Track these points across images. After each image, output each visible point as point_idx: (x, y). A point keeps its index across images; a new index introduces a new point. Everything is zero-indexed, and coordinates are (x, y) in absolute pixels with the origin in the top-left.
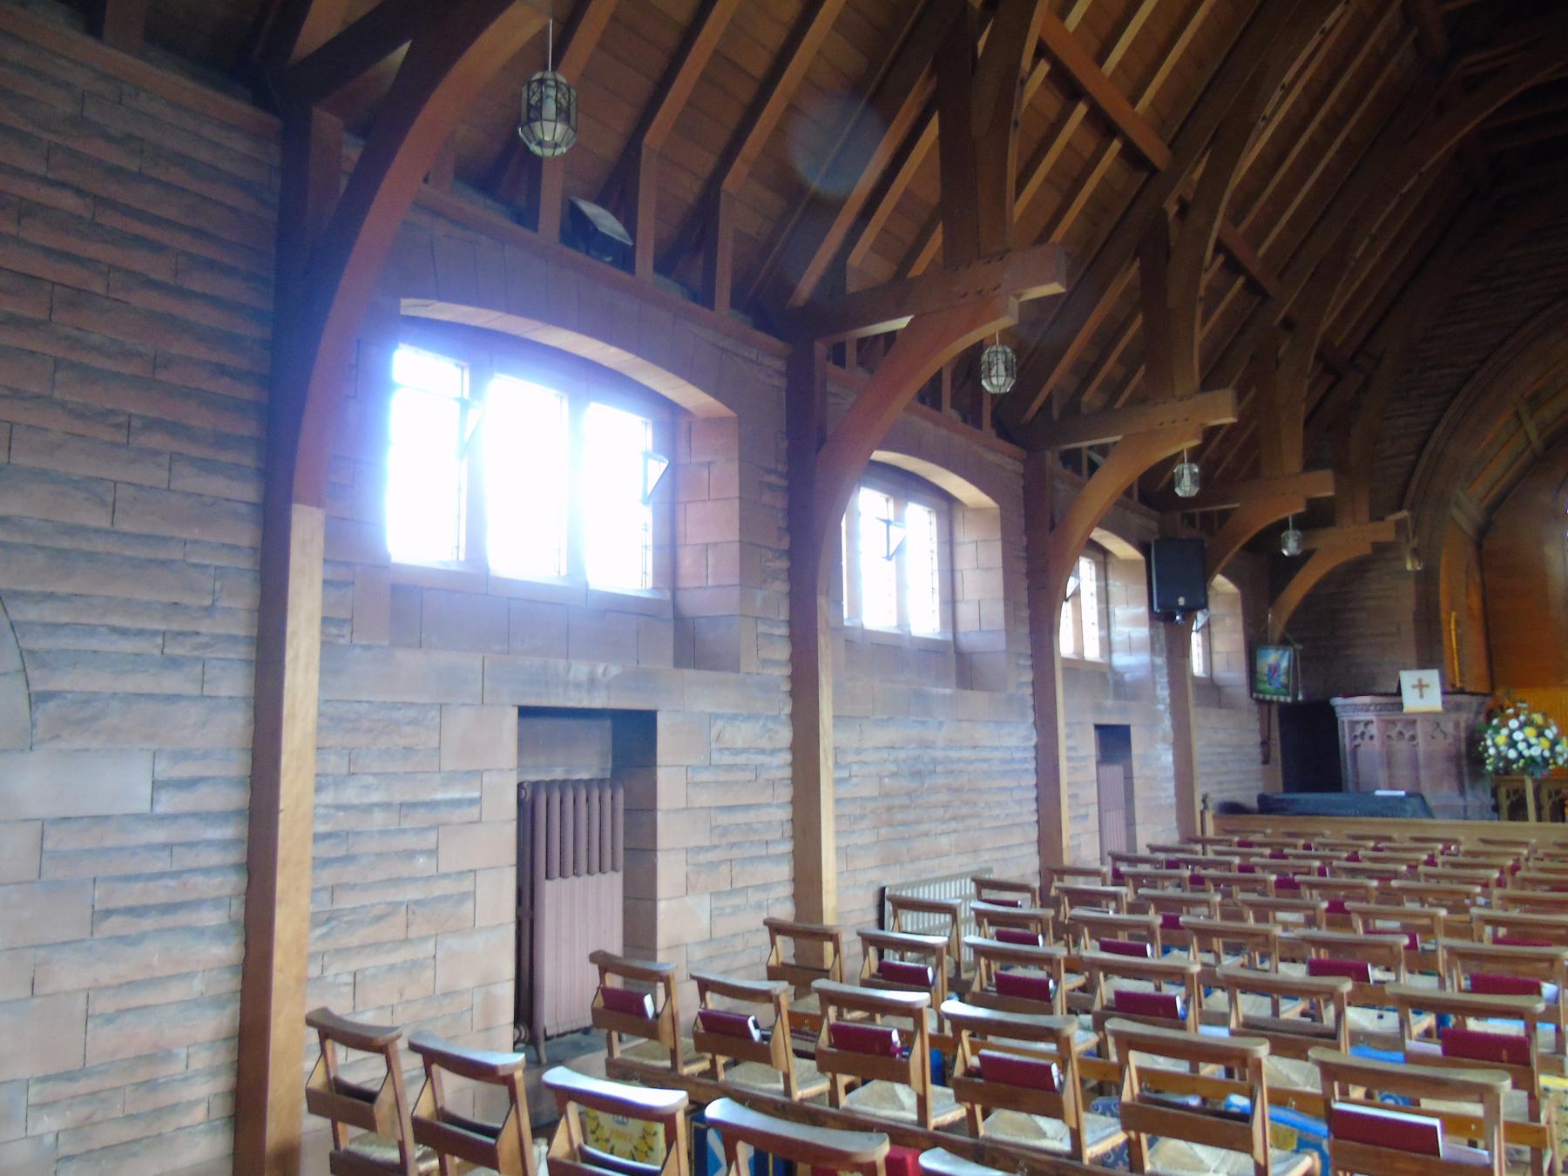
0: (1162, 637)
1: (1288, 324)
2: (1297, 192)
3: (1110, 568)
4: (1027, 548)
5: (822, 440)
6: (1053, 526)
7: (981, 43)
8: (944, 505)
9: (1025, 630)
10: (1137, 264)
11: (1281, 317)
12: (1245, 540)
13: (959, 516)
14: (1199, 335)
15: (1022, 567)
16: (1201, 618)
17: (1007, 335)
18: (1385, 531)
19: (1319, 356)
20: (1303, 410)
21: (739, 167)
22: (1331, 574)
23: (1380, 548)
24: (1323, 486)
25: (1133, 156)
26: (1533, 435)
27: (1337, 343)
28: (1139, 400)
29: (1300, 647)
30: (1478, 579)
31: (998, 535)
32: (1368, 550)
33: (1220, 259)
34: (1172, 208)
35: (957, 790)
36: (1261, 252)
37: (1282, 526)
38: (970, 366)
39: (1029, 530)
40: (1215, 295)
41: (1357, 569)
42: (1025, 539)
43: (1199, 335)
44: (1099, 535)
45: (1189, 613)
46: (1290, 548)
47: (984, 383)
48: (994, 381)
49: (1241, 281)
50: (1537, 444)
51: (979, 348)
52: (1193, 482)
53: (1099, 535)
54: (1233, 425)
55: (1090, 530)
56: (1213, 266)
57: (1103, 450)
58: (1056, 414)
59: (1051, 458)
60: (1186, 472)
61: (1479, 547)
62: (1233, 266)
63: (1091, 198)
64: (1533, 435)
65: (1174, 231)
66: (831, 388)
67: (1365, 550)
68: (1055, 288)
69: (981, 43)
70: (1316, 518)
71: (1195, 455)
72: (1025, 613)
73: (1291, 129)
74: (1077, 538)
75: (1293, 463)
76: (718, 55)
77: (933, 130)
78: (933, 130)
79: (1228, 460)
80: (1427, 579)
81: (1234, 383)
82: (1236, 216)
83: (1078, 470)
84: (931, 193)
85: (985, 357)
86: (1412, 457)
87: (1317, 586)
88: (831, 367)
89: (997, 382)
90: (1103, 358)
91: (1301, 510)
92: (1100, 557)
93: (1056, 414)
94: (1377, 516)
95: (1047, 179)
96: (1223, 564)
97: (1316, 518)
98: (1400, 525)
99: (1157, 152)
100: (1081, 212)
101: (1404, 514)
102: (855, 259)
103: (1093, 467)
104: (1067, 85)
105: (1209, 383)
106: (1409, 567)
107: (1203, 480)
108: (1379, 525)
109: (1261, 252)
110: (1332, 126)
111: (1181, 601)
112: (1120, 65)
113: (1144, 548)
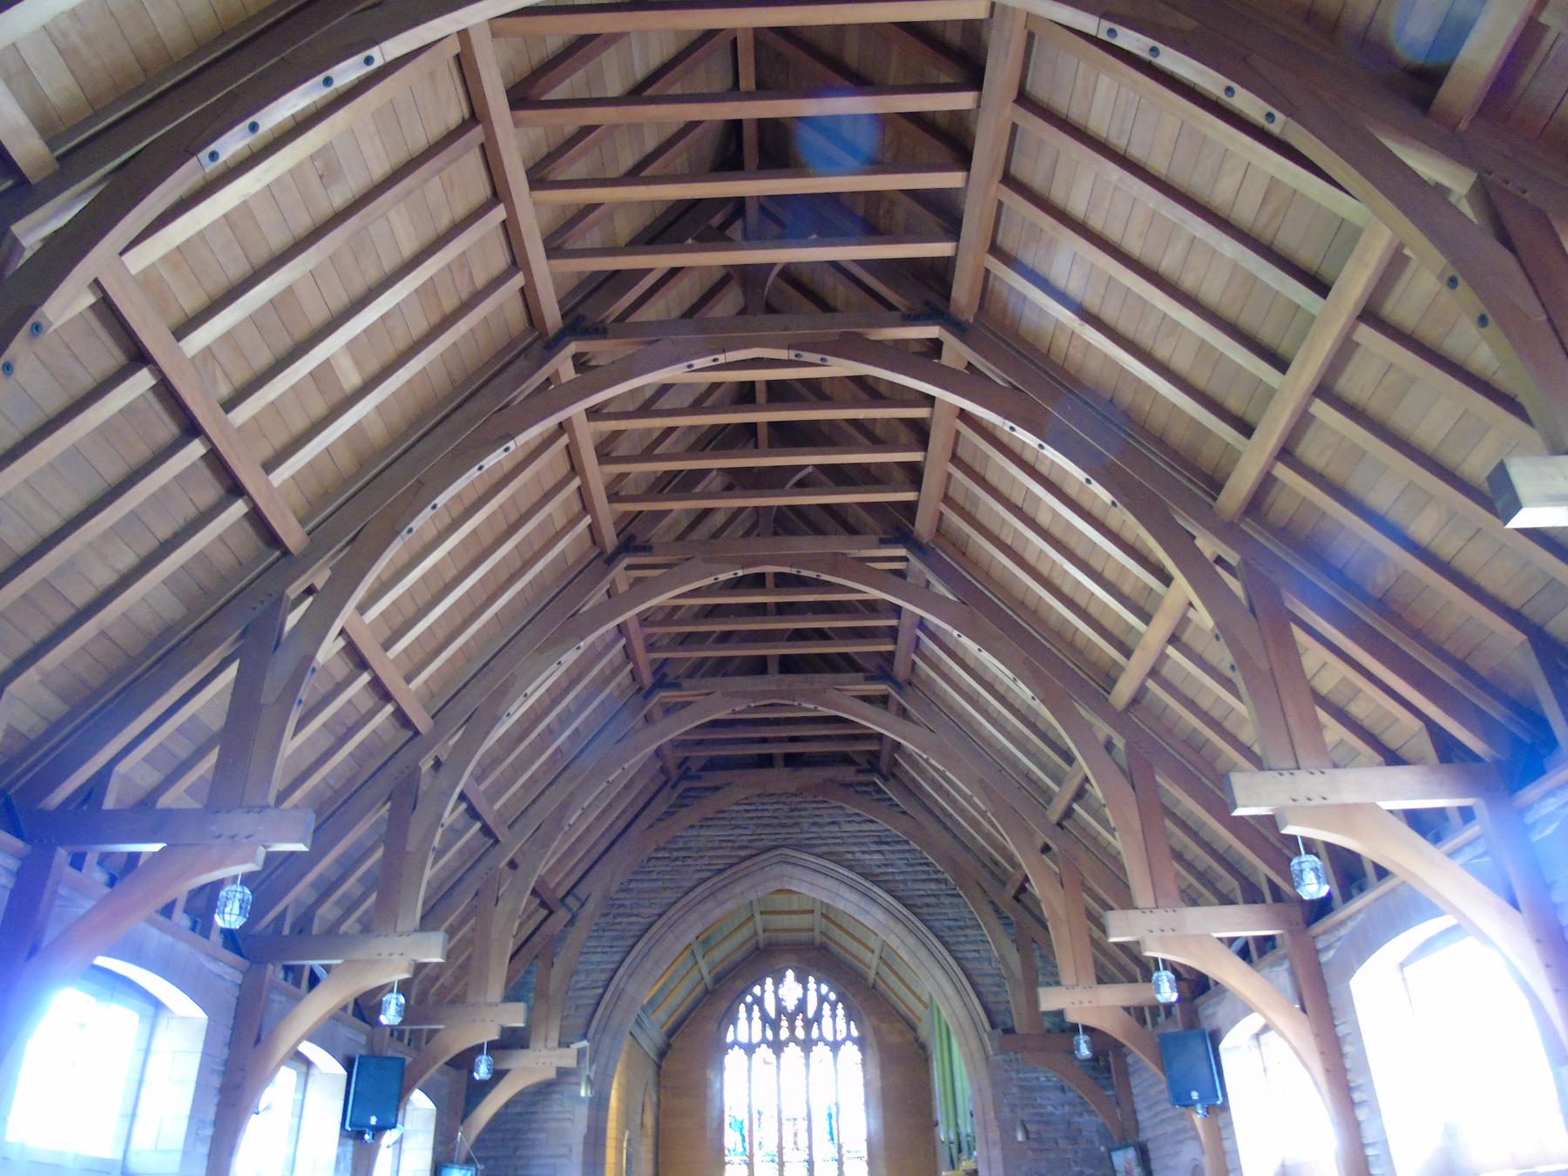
0: (349, 1155)
1: (513, 865)
2: (533, 762)
3: (311, 1080)
4: (226, 1063)
5: (34, 951)
6: (258, 1040)
7: (292, 620)
8: (150, 1010)
9: (204, 1150)
10: (388, 805)
11: (508, 859)
12: (447, 1059)
13: (163, 1022)
14: (428, 874)
15: (216, 1082)
16: (389, 1137)
17: (247, 880)
18: (568, 1058)
19: (534, 892)
20: (510, 947)
21: (31, 675)
22: (521, 1093)
23: (562, 1073)
24: (515, 1016)
25: (401, 717)
26: (705, 972)
27: (552, 886)
28: (367, 928)
29: (481, 1167)
30: (654, 1097)
31: (200, 1046)
32: (552, 1074)
33: (464, 806)
34: (426, 764)
35: (581, 319)
36: (497, 806)
37: (477, 1050)
38: (205, 901)
39: (233, 1043)
40: (454, 833)
41: (542, 1092)
42: (226, 1051)
43: (428, 874)
44: (308, 1049)
45: (379, 1131)
46: (482, 1072)
47: (217, 917)
48: (227, 917)
49: (478, 825)
50: (708, 979)
51: (218, 885)
52: (399, 1013)
53: (308, 1049)
54: (438, 964)
55: (299, 1042)
56: (451, 813)
57: (327, 968)
58: (286, 931)
59: (274, 973)
60: (394, 1002)
61: (659, 1067)
62: (473, 813)
63: (362, 743)
64: (705, 972)
65: (424, 786)
66: (63, 891)
67: (551, 1074)
68: (301, 847)
69: (292, 620)
70: (512, 1041)
71: (404, 987)
72: (208, 1132)
73: (534, 716)
74: (283, 1048)
75: (495, 990)
76: (46, 583)
77: (232, 671)
78: (232, 671)
79: (429, 995)
80: (599, 1104)
81: (446, 924)
82: (479, 778)
83: (297, 984)
84: (216, 722)
85: (223, 893)
86: (600, 991)
87: (507, 1105)
88: (69, 870)
89: (230, 917)
90: (342, 879)
91: (495, 1037)
92: (303, 1068)
93: (286, 931)
94: (564, 1044)
95: (324, 725)
96: (421, 1082)
97: (512, 1041)
98: (581, 1053)
99: (422, 721)
100: (351, 754)
101: (585, 1043)
102: (122, 768)
103: (314, 981)
104: (356, 658)
105: (429, 921)
106: (583, 1093)
107: (407, 1013)
108: (566, 1050)
109: (497, 806)
110: (582, 703)
111: (373, 1120)
112: (405, 650)
113: (348, 1064)
